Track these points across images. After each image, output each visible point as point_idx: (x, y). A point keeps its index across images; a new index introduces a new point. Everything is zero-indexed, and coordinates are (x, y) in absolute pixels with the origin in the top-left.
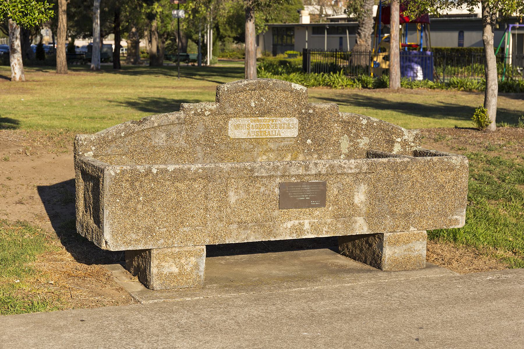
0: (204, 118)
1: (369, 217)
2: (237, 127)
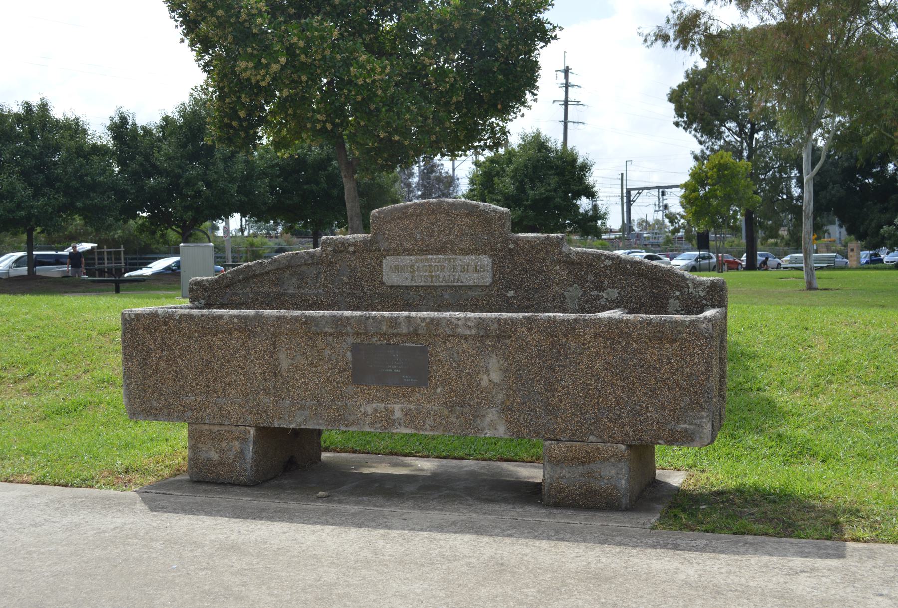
2: (397, 269)
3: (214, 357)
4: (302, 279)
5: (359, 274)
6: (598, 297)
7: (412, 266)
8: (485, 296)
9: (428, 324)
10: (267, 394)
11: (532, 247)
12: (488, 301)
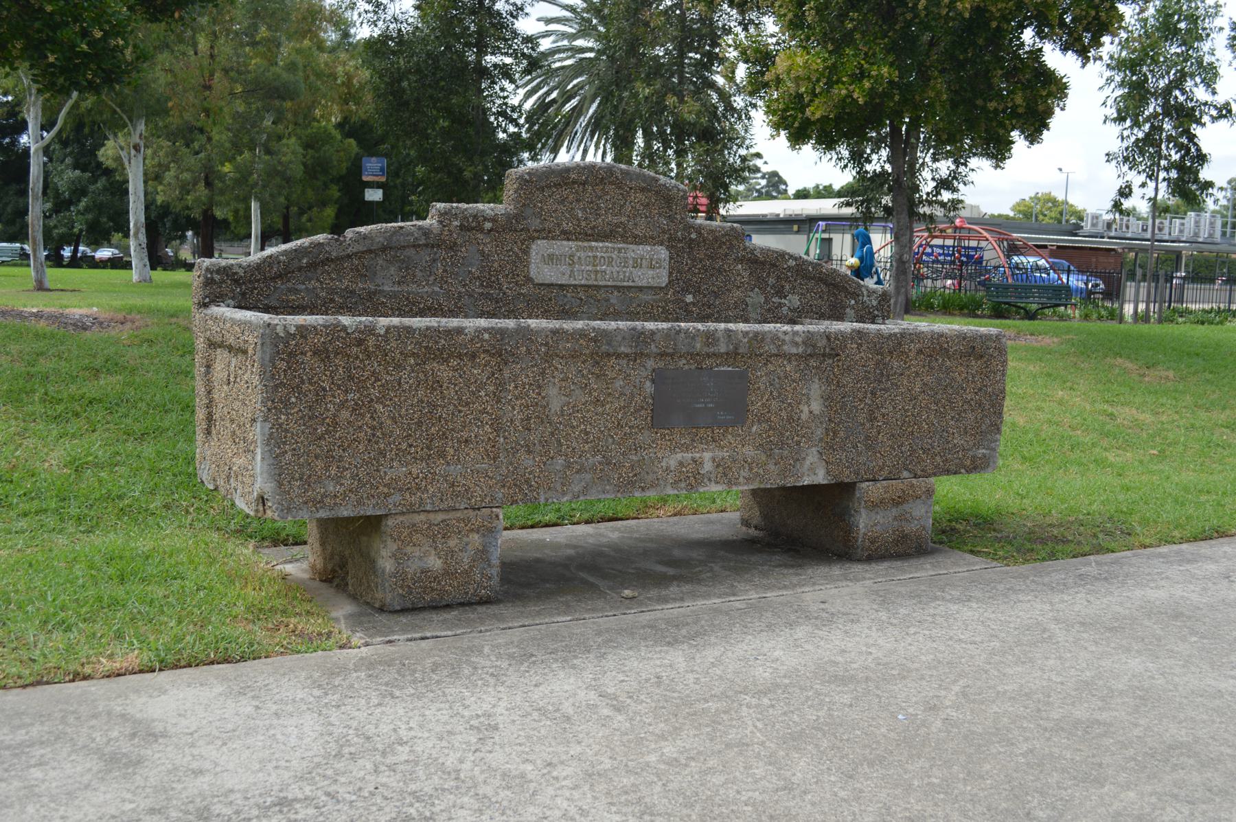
0: (480, 236)
1: (829, 448)
2: (551, 259)
3: (443, 398)
4: (407, 268)
5: (496, 265)
6: (780, 305)
7: (572, 256)
8: (660, 301)
9: (752, 339)
10: (529, 452)
11: (716, 239)
12: (663, 308)
